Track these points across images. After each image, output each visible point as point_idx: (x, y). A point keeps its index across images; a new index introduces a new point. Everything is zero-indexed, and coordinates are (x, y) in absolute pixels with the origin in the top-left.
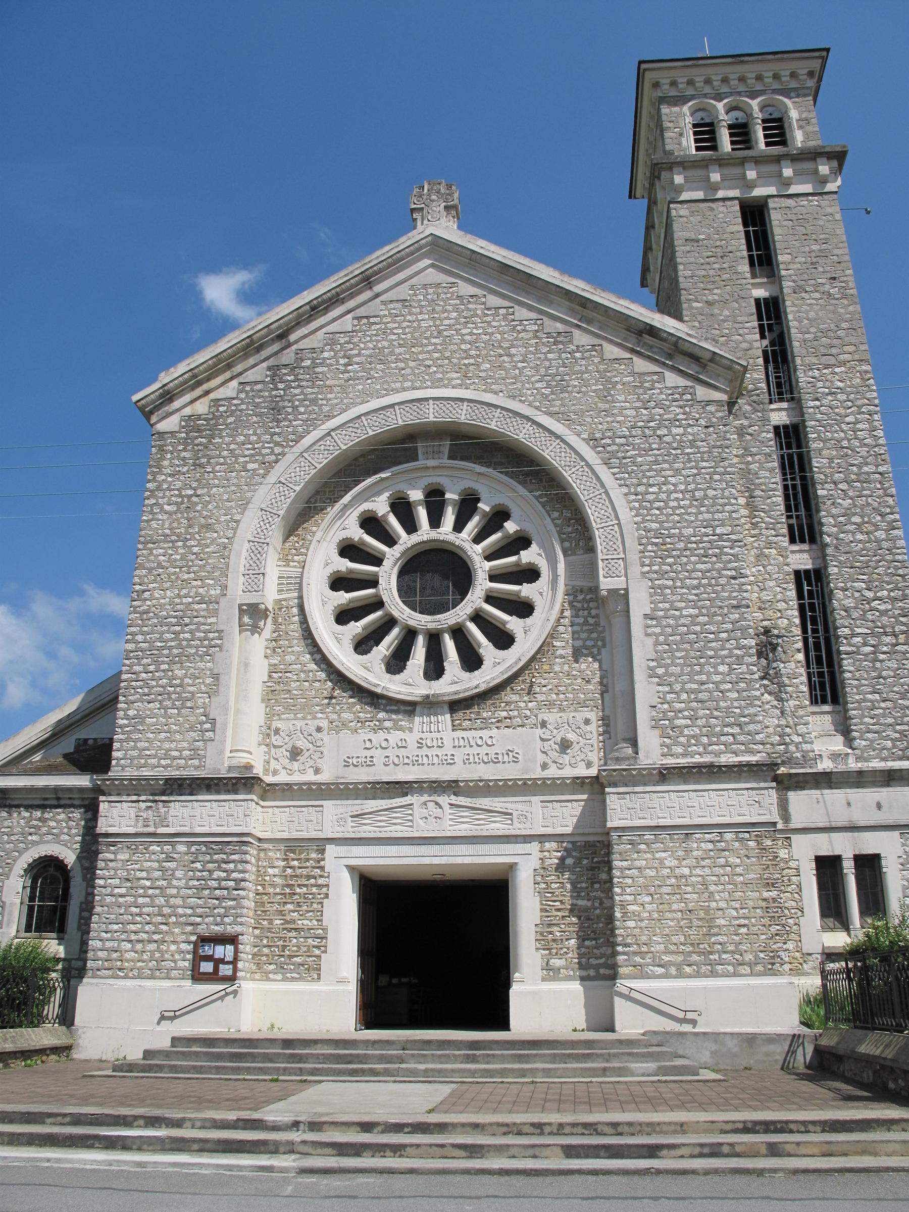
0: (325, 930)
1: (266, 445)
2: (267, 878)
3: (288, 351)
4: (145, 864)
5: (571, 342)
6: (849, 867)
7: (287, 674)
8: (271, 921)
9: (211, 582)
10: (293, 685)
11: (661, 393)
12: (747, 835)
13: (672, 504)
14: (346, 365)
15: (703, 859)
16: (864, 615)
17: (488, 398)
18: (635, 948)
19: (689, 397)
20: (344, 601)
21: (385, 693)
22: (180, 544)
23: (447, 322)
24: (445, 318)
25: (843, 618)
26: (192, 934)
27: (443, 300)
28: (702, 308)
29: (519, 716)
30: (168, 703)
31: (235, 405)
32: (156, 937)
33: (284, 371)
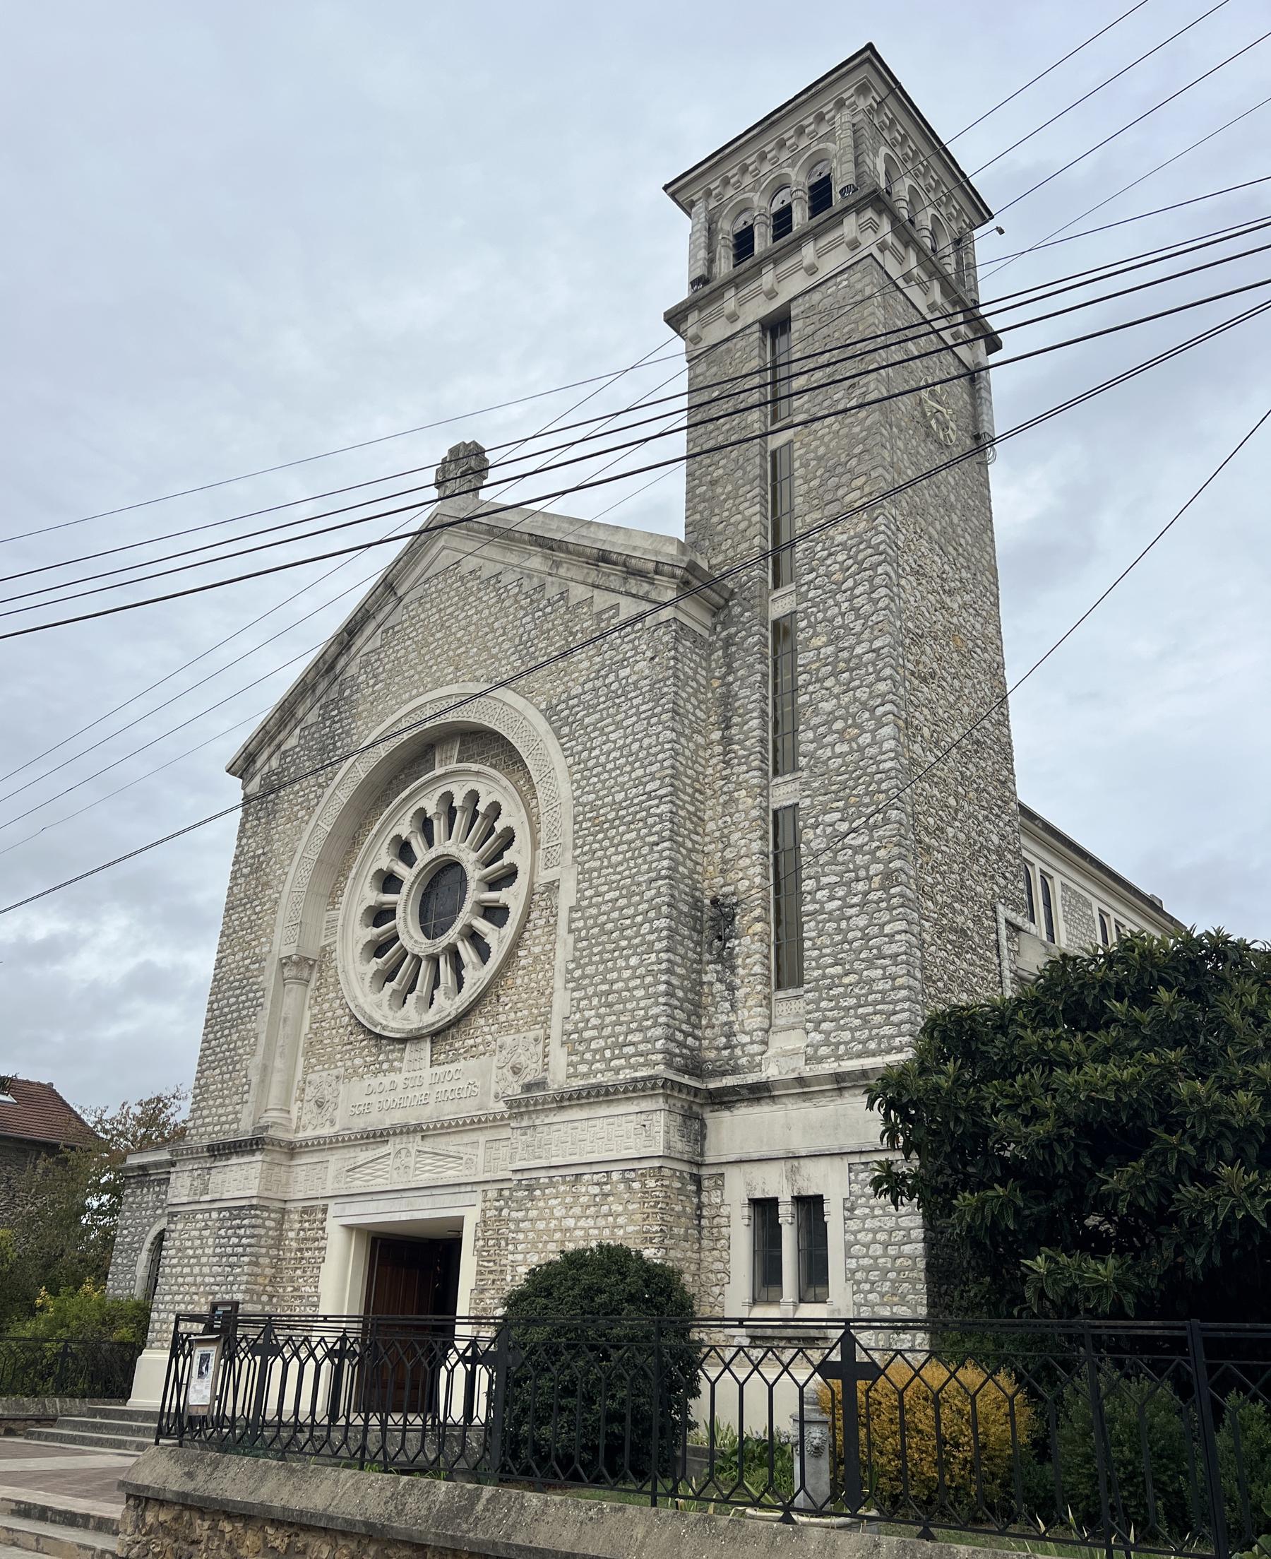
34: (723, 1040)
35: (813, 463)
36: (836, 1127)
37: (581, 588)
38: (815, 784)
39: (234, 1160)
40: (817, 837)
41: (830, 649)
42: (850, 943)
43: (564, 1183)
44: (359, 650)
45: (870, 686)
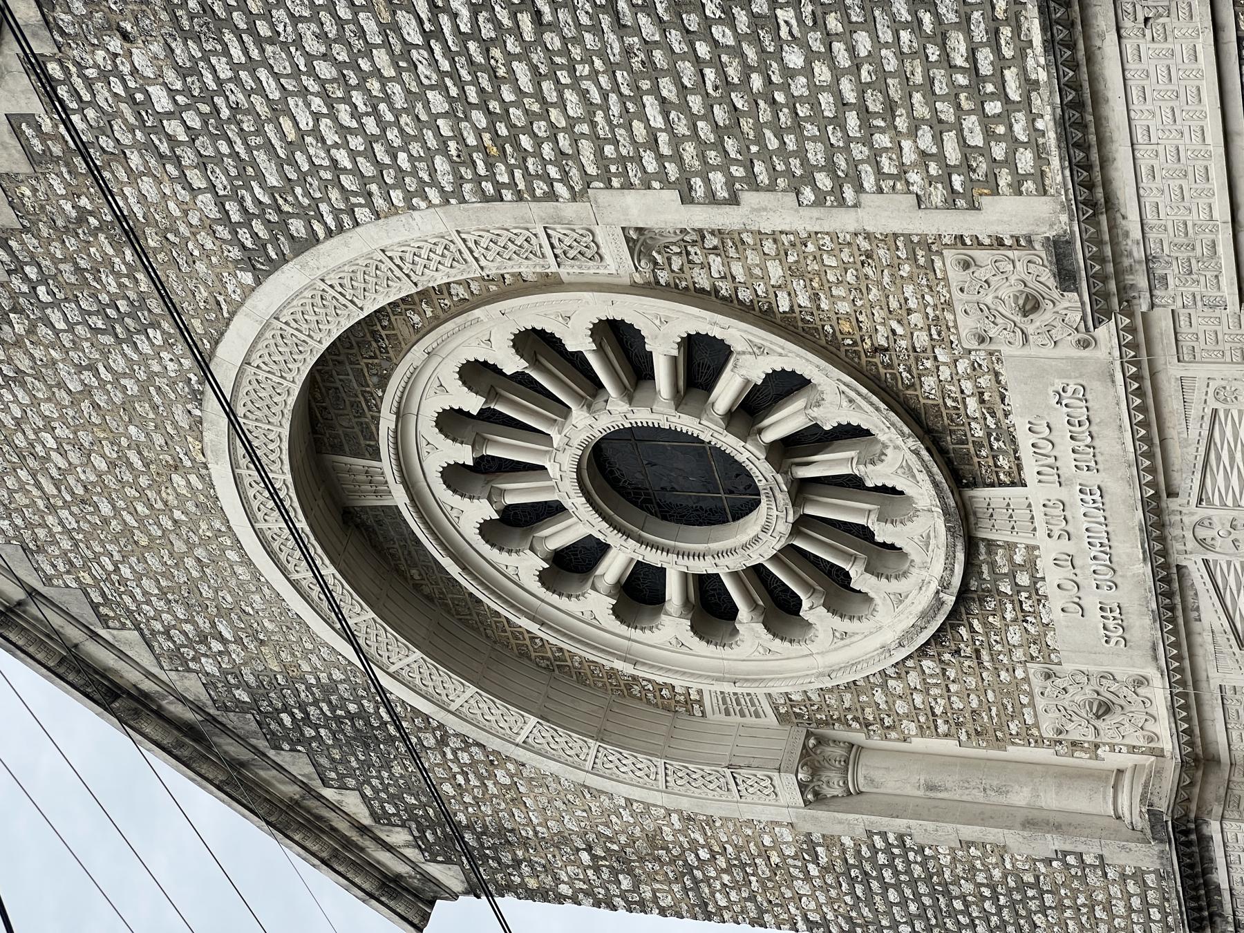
44: (148, 675)
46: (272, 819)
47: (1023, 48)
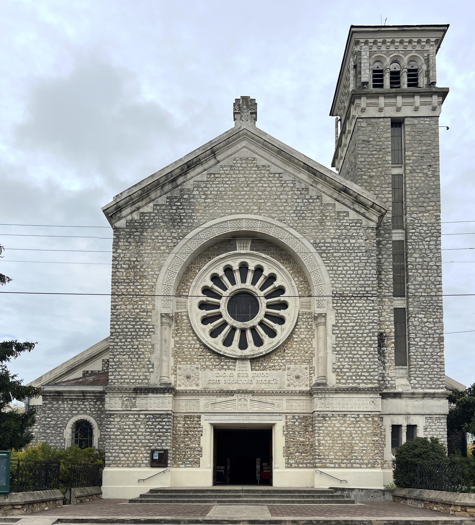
0: (201, 448)
1: (169, 238)
2: (177, 428)
3: (177, 189)
4: (127, 423)
5: (308, 194)
6: (404, 430)
7: (183, 345)
8: (179, 445)
9: (148, 303)
10: (185, 350)
11: (347, 222)
12: (368, 416)
13: (348, 276)
14: (205, 199)
15: (351, 424)
16: (422, 329)
17: (270, 220)
18: (322, 457)
19: (359, 225)
20: (205, 314)
21: (224, 354)
22: (132, 284)
23: (251, 179)
24: (251, 177)
25: (413, 329)
26: (148, 450)
27: (249, 167)
28: (367, 179)
29: (278, 365)
30: (132, 356)
31: (153, 216)
32: (134, 451)
33: (175, 200)
34: (381, 378)
35: (414, 189)
36: (423, 407)
37: (329, 198)
38: (415, 304)
39: (150, 395)
40: (415, 321)
41: (421, 260)
42: (427, 356)
43: (339, 416)
44: (192, 177)
45: (435, 277)
46: (146, 188)
47: (366, 384)
